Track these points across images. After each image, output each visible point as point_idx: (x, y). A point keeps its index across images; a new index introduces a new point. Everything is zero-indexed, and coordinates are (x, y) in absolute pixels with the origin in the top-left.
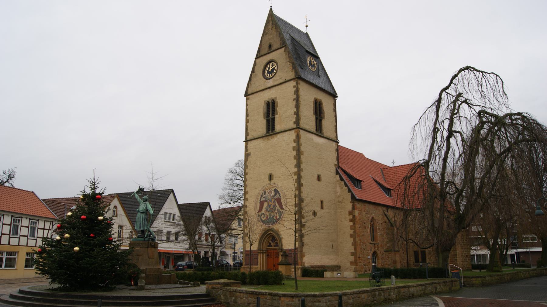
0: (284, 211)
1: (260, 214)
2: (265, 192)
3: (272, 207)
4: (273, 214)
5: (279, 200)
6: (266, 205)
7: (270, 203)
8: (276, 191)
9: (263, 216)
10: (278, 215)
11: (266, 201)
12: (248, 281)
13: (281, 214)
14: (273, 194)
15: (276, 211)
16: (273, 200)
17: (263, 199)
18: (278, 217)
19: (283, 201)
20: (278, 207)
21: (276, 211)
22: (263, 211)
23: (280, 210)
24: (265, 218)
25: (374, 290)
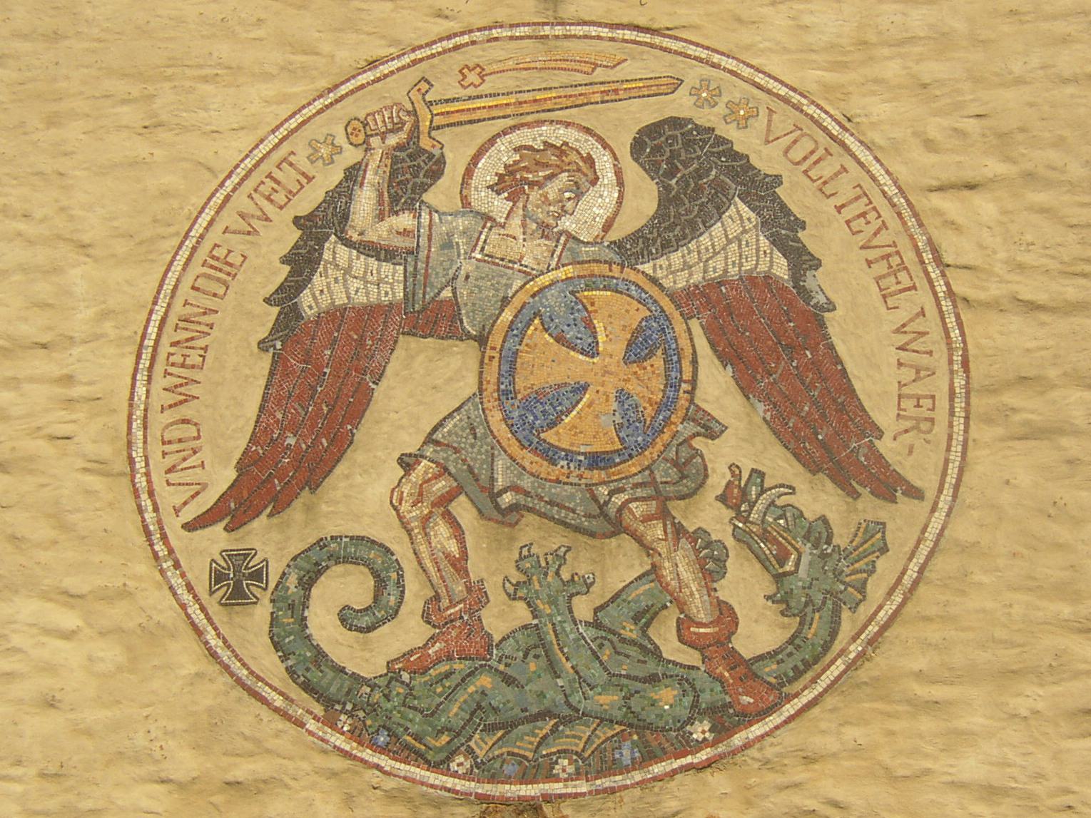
0: (901, 520)
1: (273, 542)
2: (412, 173)
3: (586, 427)
4: (620, 567)
5: (778, 340)
6: (420, 390)
7: (546, 363)
8: (692, 169)
9: (346, 586)
10: (744, 585)
11: (433, 318)
12: (802, 667)
13: (823, 589)
14: (617, 199)
15: (709, 516)
16: (614, 319)
17: (345, 281)
18: (759, 633)
19: (867, 343)
20: (741, 441)
21: (709, 516)
22: (364, 493)
23: (817, 499)
24: (407, 633)
25: (584, 638)
